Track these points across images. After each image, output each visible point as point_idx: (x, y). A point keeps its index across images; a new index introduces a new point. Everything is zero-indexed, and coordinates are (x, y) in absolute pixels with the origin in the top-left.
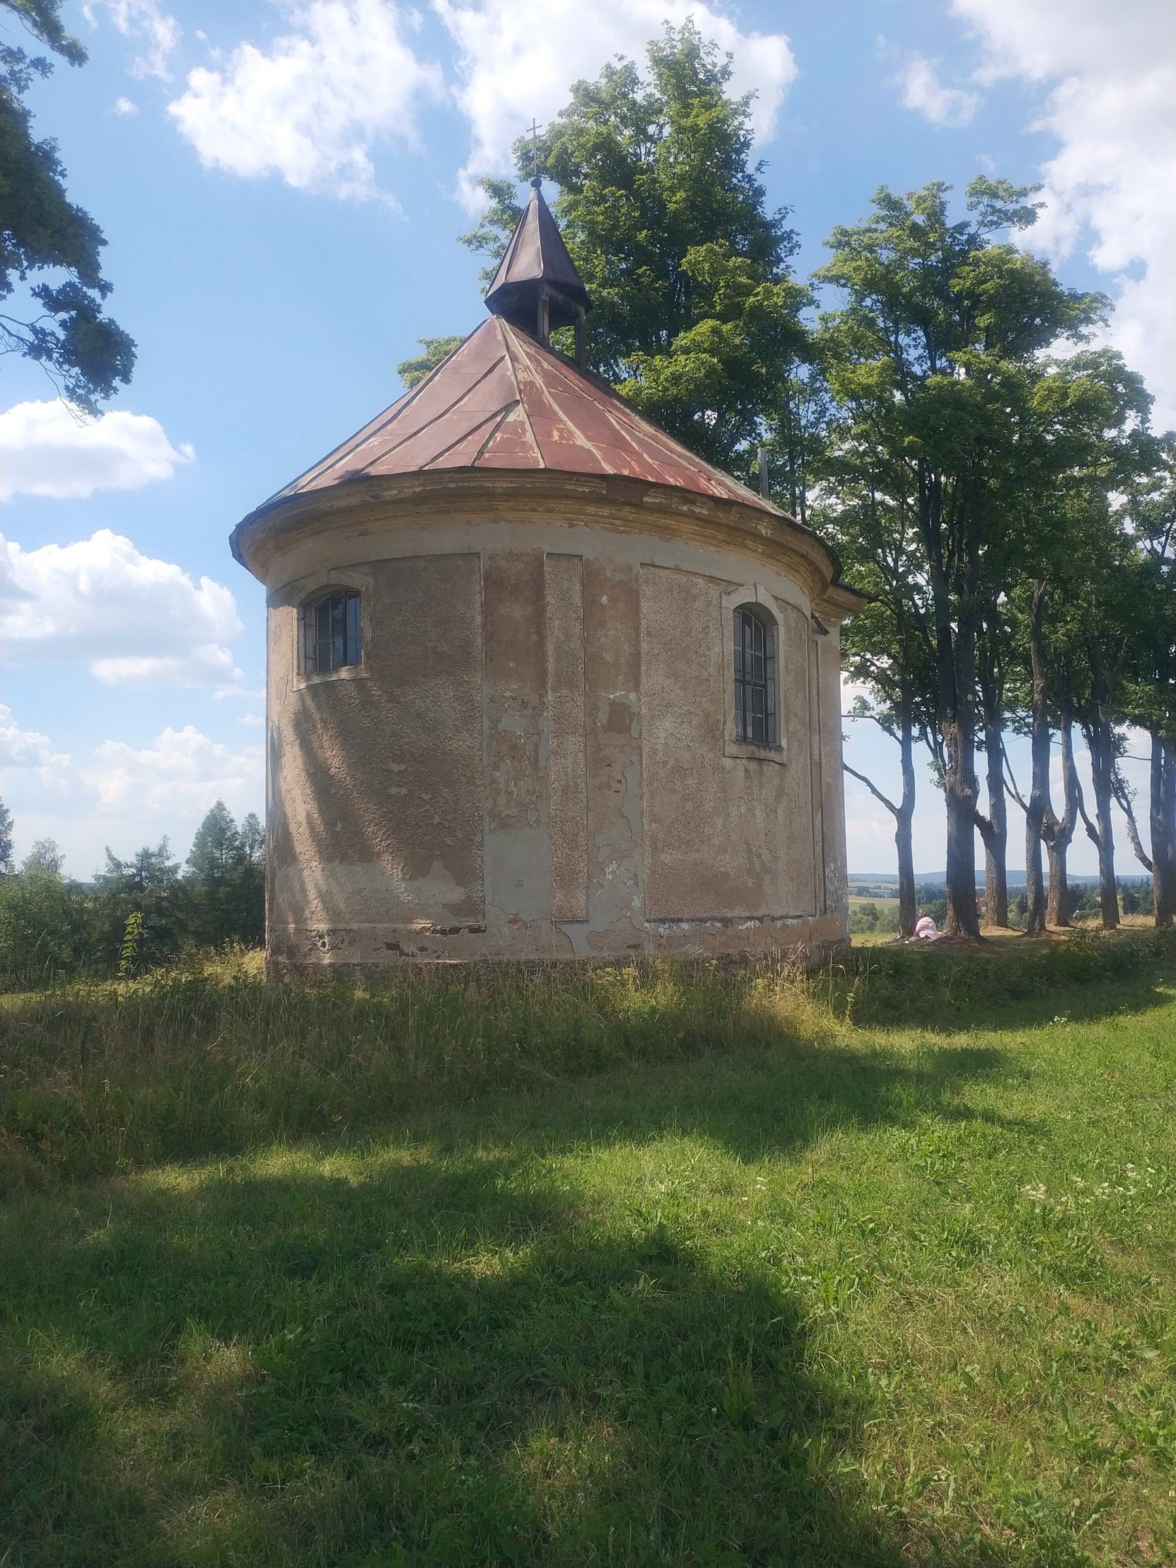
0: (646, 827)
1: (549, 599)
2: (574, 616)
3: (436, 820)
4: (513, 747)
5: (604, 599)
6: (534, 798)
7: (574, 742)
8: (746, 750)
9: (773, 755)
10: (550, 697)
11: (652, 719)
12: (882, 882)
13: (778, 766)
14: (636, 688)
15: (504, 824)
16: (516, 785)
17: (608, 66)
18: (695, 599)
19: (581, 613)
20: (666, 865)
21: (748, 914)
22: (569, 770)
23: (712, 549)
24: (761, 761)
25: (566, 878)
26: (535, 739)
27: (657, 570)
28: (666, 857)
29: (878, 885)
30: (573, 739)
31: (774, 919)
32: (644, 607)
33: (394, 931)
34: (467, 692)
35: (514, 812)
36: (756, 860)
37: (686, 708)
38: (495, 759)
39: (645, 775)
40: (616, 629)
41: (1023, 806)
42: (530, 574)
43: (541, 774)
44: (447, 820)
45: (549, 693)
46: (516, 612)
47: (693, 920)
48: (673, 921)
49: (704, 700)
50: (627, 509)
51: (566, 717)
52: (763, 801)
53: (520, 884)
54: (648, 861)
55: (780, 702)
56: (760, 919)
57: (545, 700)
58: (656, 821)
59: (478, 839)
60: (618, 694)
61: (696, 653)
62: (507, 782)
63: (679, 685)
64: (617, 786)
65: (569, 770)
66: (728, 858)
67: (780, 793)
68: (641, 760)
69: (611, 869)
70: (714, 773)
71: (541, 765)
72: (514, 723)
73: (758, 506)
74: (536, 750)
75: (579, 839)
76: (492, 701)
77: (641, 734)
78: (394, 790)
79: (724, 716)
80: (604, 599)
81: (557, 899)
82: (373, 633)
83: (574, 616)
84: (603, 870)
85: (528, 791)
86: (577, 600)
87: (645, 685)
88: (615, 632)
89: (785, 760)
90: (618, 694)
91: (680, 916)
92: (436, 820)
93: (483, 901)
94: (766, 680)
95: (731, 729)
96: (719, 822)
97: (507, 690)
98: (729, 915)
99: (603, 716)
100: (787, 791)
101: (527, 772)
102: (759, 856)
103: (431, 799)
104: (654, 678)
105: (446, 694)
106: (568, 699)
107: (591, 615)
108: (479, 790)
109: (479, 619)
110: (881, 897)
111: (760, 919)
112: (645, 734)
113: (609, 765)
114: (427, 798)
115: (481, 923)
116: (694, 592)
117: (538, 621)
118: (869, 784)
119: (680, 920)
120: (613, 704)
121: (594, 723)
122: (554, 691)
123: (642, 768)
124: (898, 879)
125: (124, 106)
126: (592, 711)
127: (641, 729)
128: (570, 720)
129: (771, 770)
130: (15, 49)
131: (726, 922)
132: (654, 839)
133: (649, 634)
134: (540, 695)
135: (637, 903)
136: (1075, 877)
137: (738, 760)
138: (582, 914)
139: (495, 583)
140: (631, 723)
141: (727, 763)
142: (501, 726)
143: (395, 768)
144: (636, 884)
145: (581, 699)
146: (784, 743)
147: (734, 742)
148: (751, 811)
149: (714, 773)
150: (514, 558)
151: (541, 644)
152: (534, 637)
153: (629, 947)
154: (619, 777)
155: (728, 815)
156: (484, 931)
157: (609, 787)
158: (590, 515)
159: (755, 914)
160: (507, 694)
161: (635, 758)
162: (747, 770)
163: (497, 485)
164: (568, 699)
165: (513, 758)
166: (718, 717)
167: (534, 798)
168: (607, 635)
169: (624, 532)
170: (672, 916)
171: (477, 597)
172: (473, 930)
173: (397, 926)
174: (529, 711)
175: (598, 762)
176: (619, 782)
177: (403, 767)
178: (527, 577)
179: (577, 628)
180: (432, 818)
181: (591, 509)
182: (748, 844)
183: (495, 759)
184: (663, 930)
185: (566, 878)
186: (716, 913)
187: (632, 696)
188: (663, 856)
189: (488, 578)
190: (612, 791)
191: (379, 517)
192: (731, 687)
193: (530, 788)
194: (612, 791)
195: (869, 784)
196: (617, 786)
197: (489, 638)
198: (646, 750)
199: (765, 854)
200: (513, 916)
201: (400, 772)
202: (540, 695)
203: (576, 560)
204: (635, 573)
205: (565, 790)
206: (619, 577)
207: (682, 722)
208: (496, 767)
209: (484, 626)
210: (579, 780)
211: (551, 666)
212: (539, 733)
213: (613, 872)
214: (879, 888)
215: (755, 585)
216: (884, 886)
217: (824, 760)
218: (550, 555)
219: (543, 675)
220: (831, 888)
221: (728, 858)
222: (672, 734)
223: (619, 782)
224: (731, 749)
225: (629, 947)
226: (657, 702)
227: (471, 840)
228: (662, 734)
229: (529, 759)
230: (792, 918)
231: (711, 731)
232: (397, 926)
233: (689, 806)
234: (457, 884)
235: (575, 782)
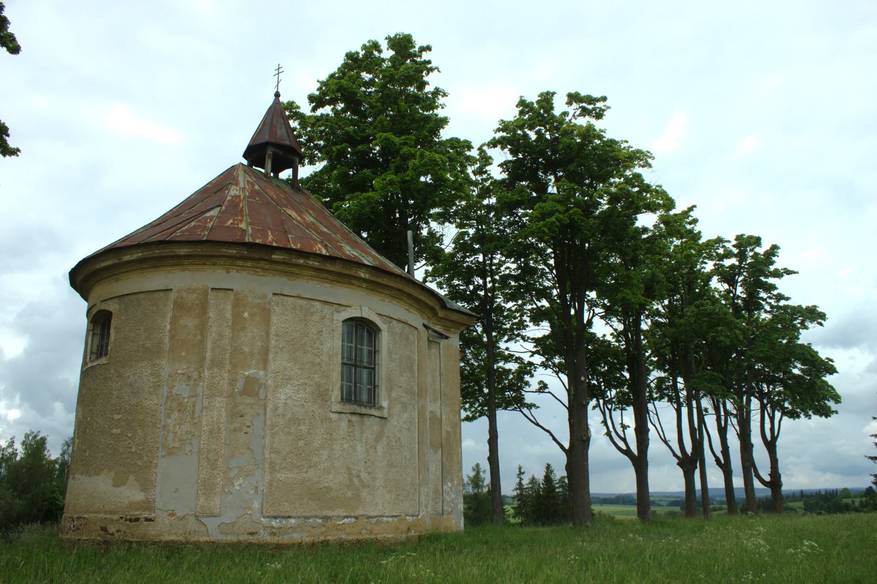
0: (267, 456)
1: (211, 315)
2: (226, 325)
3: (134, 450)
4: (181, 404)
5: (246, 315)
6: (190, 436)
7: (220, 402)
8: (349, 408)
9: (373, 412)
10: (206, 373)
11: (276, 387)
12: (664, 496)
13: (379, 419)
14: (265, 368)
15: (171, 452)
16: (180, 428)
17: (546, 99)
18: (312, 314)
19: (230, 323)
20: (281, 481)
21: (346, 514)
22: (215, 419)
23: (327, 285)
24: (362, 415)
25: (207, 487)
26: (194, 399)
27: (285, 297)
28: (281, 476)
29: (661, 498)
30: (219, 399)
31: (369, 517)
32: (274, 319)
33: (105, 519)
34: (158, 370)
35: (177, 445)
36: (356, 480)
37: (302, 381)
38: (169, 412)
39: (268, 423)
40: (252, 332)
41: (562, 447)
42: (200, 300)
43: (196, 421)
44: (139, 449)
45: (206, 371)
46: (189, 322)
47: (299, 517)
48: (283, 517)
49: (316, 376)
50: (262, 262)
51: (215, 386)
52: (364, 441)
53: (177, 491)
54: (267, 478)
55: (382, 379)
56: (356, 518)
57: (202, 375)
58: (275, 452)
59: (155, 462)
60: (251, 371)
61: (312, 347)
62: (175, 426)
63: (298, 366)
64: (246, 429)
65: (215, 419)
66: (331, 477)
67: (379, 437)
68: (265, 414)
69: (238, 483)
70: (322, 422)
71: (196, 415)
72: (182, 389)
73: (359, 261)
74: (194, 406)
75: (219, 463)
76: (170, 376)
77: (266, 397)
78: (114, 431)
79: (332, 386)
80: (246, 315)
81: (201, 501)
82: (115, 336)
83: (226, 325)
84: (233, 483)
85: (187, 432)
86: (228, 315)
87: (272, 366)
88: (251, 334)
89: (385, 413)
90: (251, 371)
91: (290, 515)
92: (134, 450)
93: (154, 502)
94: (375, 365)
95: (336, 394)
96: (325, 454)
97: (179, 369)
98: (330, 514)
99: (240, 385)
100: (386, 434)
101: (187, 420)
102: (358, 476)
103: (132, 436)
104: (279, 362)
105: (146, 372)
106: (217, 374)
107: (238, 323)
108: (158, 430)
109: (168, 327)
110: (662, 506)
111: (356, 518)
112: (269, 397)
113: (242, 416)
114: (129, 435)
115: (153, 515)
116: (312, 310)
117: (202, 328)
118: (551, 434)
119: (289, 517)
120: (247, 377)
121: (233, 389)
122: (209, 370)
123: (265, 418)
124: (724, 493)
125: (419, 147)
126: (233, 382)
127: (266, 394)
128: (218, 387)
129: (371, 424)
130: (478, 152)
131: (326, 518)
132: (272, 464)
133: (277, 335)
134: (199, 372)
135: (256, 505)
136: (652, 493)
137: (343, 415)
138: (217, 511)
139: (180, 307)
140: (259, 389)
141: (334, 416)
142: (174, 391)
143: (116, 417)
144: (256, 492)
145: (226, 375)
146: (385, 404)
147: (339, 403)
148: (354, 447)
149: (322, 422)
150: (192, 291)
151: (203, 341)
152: (199, 337)
153: (250, 534)
154: (248, 424)
155: (332, 449)
156: (153, 521)
157: (240, 430)
158: (239, 266)
159: (353, 514)
160: (180, 372)
161: (261, 412)
162: (350, 421)
163: (181, 250)
164: (217, 374)
165: (180, 411)
166: (327, 387)
167: (190, 436)
168: (246, 336)
169: (263, 275)
170: (283, 514)
171: (169, 314)
172: (147, 520)
173: (107, 516)
174: (192, 382)
175: (235, 414)
176: (249, 427)
177: (120, 416)
178: (198, 302)
179: (227, 332)
180: (131, 448)
181: (240, 263)
182: (349, 469)
183: (169, 412)
184: (274, 523)
185: (207, 487)
186: (319, 513)
187: (262, 373)
188: (278, 475)
189: (175, 303)
190: (243, 433)
191: (123, 271)
192: (338, 368)
193: (189, 430)
194: (243, 433)
195: (551, 434)
196: (246, 429)
197: (172, 338)
198: (270, 406)
199: (364, 475)
200: (171, 512)
201: (118, 419)
202: (199, 372)
203: (230, 292)
204: (268, 299)
205: (211, 431)
206: (257, 301)
207: (299, 390)
208: (169, 416)
209: (170, 331)
210: (221, 425)
211: (208, 355)
212: (196, 396)
213: (240, 485)
214: (662, 500)
215: (361, 307)
216: (664, 499)
217: (444, 417)
218: (213, 289)
219: (203, 359)
220: (447, 498)
221: (331, 477)
222: (290, 397)
223: (249, 427)
224: (337, 407)
225: (250, 534)
226: (281, 377)
227: (151, 462)
228: (283, 397)
229: (189, 412)
230: (387, 517)
231: (322, 395)
232: (107, 516)
233: (301, 443)
234: (141, 490)
235: (218, 427)
